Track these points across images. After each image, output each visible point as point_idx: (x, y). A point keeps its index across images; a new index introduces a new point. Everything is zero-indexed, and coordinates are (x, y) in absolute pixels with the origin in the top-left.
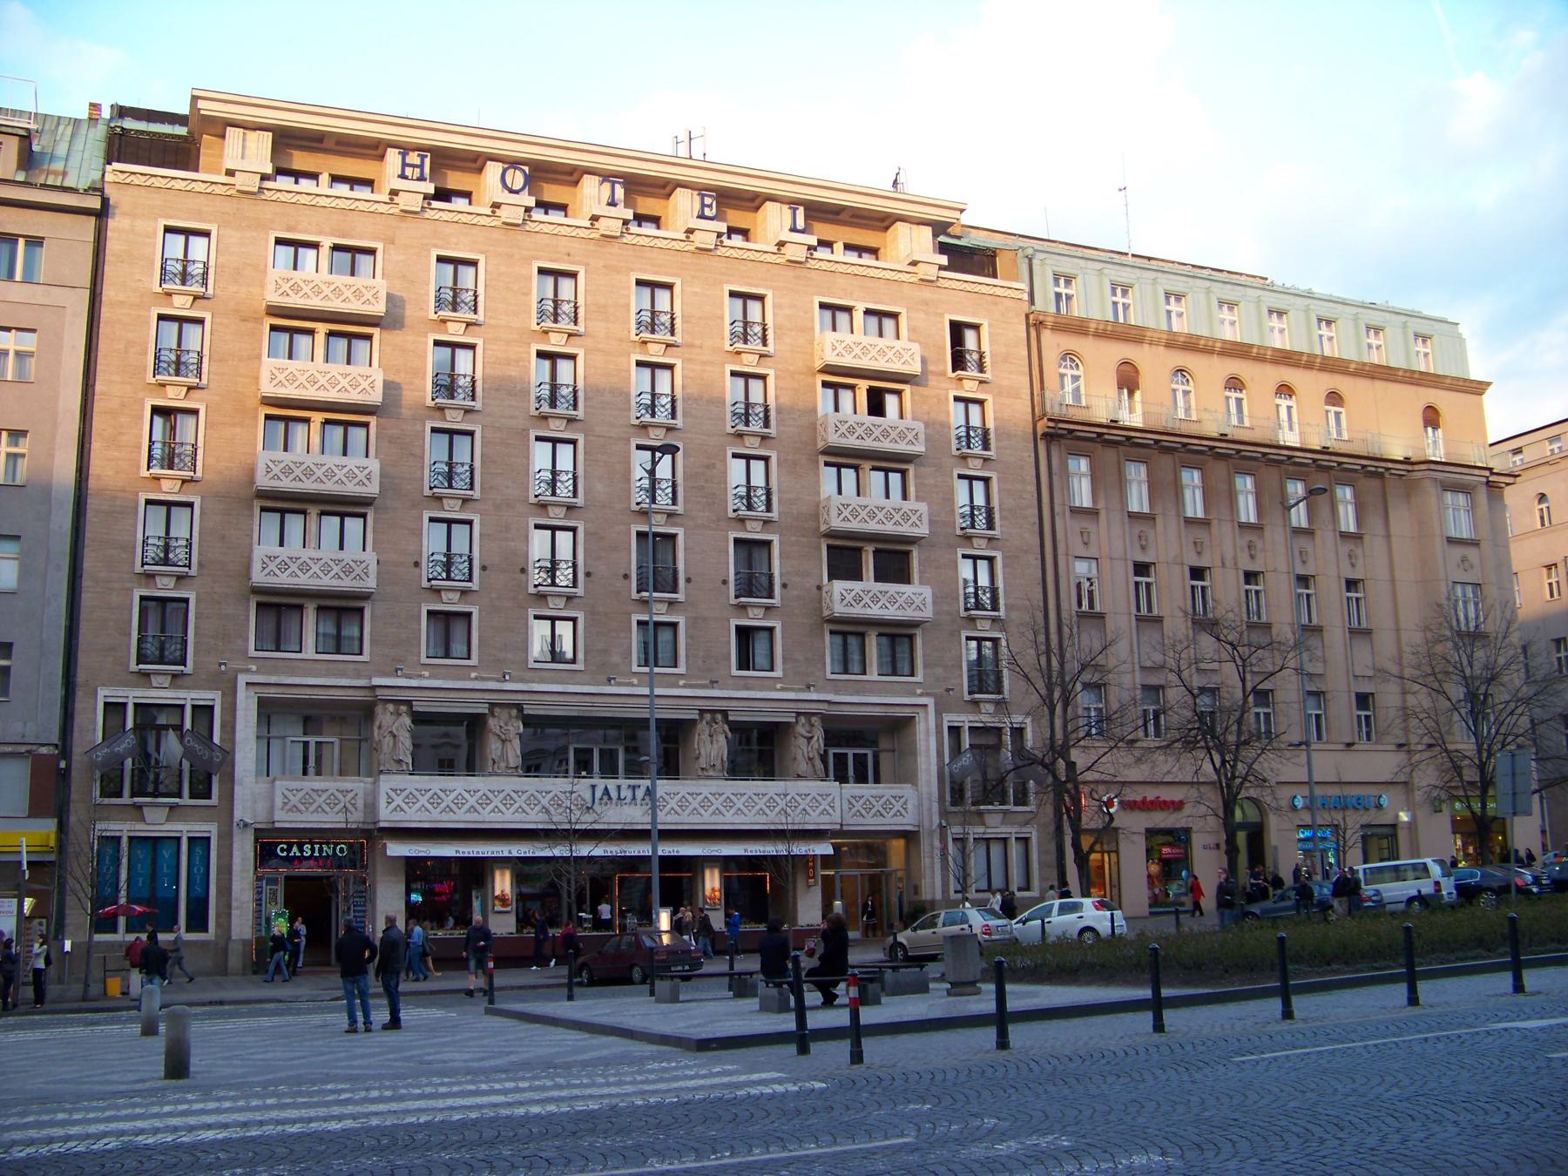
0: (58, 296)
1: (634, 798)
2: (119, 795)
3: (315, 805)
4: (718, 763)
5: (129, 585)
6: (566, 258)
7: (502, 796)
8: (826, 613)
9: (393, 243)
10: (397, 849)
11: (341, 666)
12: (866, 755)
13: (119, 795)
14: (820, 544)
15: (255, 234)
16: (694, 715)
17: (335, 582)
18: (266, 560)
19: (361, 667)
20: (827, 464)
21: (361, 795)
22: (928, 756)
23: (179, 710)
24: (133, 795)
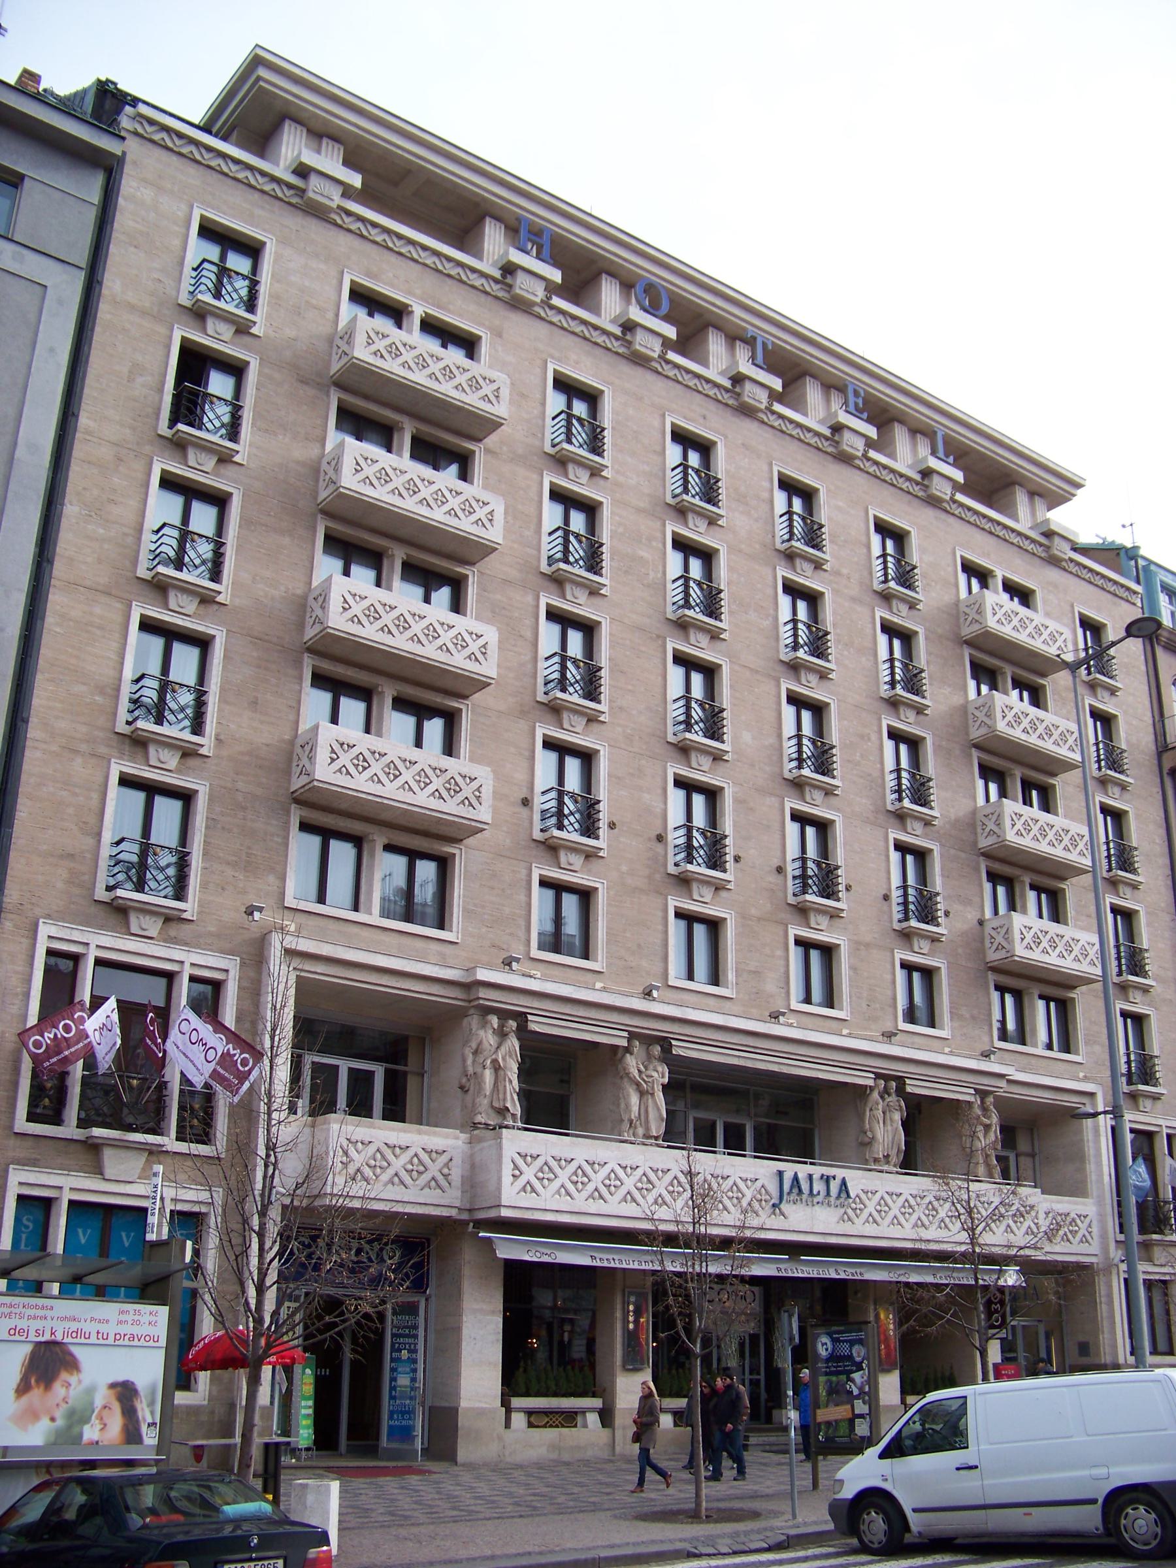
0: (32, 265)
1: (828, 1194)
2: (56, 1118)
3: (390, 1172)
4: (893, 1153)
5: (103, 750)
6: (702, 421)
7: (572, 1167)
8: (993, 956)
9: (500, 335)
10: (511, 1249)
11: (419, 944)
12: (372, 1073)
13: (56, 1118)
14: (978, 864)
15: (322, 266)
16: (867, 1080)
17: (434, 804)
18: (336, 747)
19: (448, 949)
20: (305, 827)
21: (457, 1161)
22: (1099, 1164)
23: (163, 982)
24: (83, 1123)
